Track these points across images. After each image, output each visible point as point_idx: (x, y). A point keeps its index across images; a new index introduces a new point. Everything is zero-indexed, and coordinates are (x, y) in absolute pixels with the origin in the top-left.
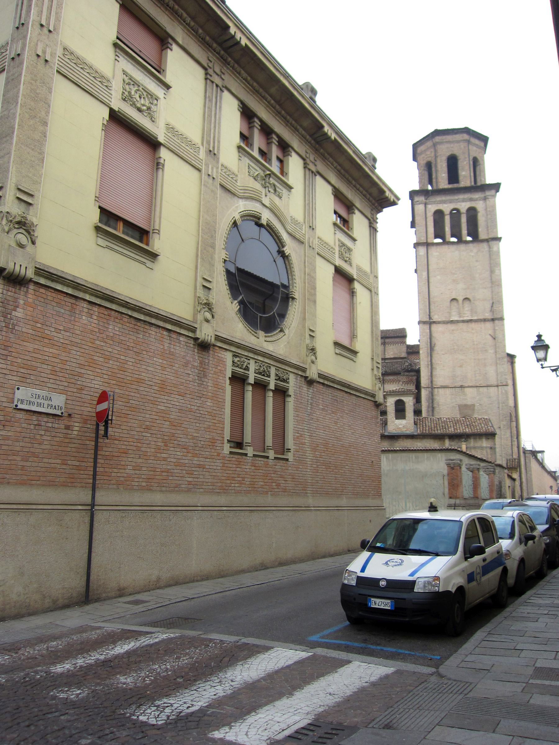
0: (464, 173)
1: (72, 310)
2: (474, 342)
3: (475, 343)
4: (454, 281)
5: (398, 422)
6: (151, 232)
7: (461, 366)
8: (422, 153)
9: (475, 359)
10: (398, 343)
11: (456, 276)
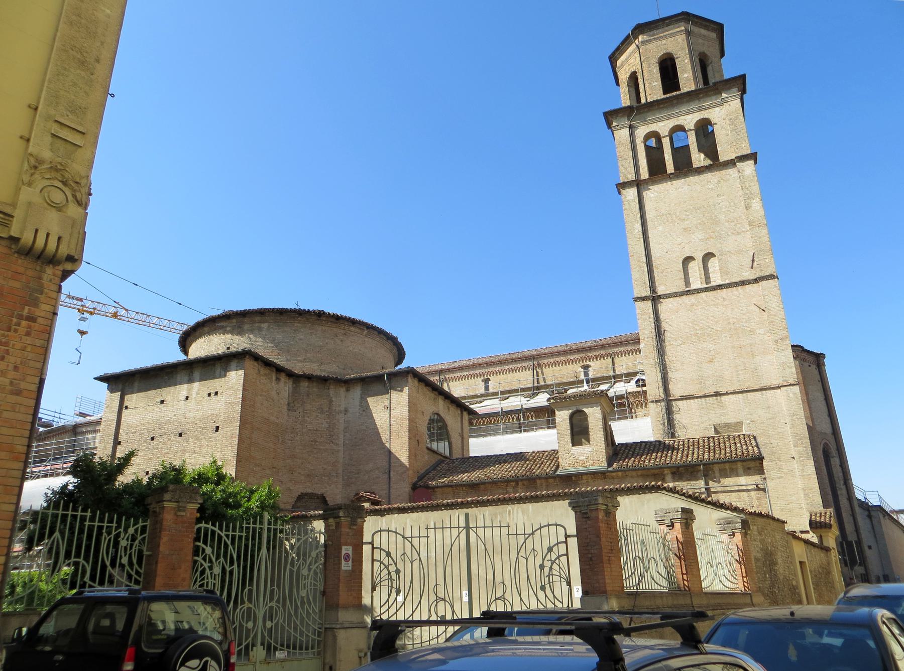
0: (685, 75)
1: (278, 379)
2: (729, 319)
3: (731, 320)
4: (685, 230)
5: (577, 450)
7: (711, 361)
8: (622, 65)
9: (733, 347)
11: (688, 222)
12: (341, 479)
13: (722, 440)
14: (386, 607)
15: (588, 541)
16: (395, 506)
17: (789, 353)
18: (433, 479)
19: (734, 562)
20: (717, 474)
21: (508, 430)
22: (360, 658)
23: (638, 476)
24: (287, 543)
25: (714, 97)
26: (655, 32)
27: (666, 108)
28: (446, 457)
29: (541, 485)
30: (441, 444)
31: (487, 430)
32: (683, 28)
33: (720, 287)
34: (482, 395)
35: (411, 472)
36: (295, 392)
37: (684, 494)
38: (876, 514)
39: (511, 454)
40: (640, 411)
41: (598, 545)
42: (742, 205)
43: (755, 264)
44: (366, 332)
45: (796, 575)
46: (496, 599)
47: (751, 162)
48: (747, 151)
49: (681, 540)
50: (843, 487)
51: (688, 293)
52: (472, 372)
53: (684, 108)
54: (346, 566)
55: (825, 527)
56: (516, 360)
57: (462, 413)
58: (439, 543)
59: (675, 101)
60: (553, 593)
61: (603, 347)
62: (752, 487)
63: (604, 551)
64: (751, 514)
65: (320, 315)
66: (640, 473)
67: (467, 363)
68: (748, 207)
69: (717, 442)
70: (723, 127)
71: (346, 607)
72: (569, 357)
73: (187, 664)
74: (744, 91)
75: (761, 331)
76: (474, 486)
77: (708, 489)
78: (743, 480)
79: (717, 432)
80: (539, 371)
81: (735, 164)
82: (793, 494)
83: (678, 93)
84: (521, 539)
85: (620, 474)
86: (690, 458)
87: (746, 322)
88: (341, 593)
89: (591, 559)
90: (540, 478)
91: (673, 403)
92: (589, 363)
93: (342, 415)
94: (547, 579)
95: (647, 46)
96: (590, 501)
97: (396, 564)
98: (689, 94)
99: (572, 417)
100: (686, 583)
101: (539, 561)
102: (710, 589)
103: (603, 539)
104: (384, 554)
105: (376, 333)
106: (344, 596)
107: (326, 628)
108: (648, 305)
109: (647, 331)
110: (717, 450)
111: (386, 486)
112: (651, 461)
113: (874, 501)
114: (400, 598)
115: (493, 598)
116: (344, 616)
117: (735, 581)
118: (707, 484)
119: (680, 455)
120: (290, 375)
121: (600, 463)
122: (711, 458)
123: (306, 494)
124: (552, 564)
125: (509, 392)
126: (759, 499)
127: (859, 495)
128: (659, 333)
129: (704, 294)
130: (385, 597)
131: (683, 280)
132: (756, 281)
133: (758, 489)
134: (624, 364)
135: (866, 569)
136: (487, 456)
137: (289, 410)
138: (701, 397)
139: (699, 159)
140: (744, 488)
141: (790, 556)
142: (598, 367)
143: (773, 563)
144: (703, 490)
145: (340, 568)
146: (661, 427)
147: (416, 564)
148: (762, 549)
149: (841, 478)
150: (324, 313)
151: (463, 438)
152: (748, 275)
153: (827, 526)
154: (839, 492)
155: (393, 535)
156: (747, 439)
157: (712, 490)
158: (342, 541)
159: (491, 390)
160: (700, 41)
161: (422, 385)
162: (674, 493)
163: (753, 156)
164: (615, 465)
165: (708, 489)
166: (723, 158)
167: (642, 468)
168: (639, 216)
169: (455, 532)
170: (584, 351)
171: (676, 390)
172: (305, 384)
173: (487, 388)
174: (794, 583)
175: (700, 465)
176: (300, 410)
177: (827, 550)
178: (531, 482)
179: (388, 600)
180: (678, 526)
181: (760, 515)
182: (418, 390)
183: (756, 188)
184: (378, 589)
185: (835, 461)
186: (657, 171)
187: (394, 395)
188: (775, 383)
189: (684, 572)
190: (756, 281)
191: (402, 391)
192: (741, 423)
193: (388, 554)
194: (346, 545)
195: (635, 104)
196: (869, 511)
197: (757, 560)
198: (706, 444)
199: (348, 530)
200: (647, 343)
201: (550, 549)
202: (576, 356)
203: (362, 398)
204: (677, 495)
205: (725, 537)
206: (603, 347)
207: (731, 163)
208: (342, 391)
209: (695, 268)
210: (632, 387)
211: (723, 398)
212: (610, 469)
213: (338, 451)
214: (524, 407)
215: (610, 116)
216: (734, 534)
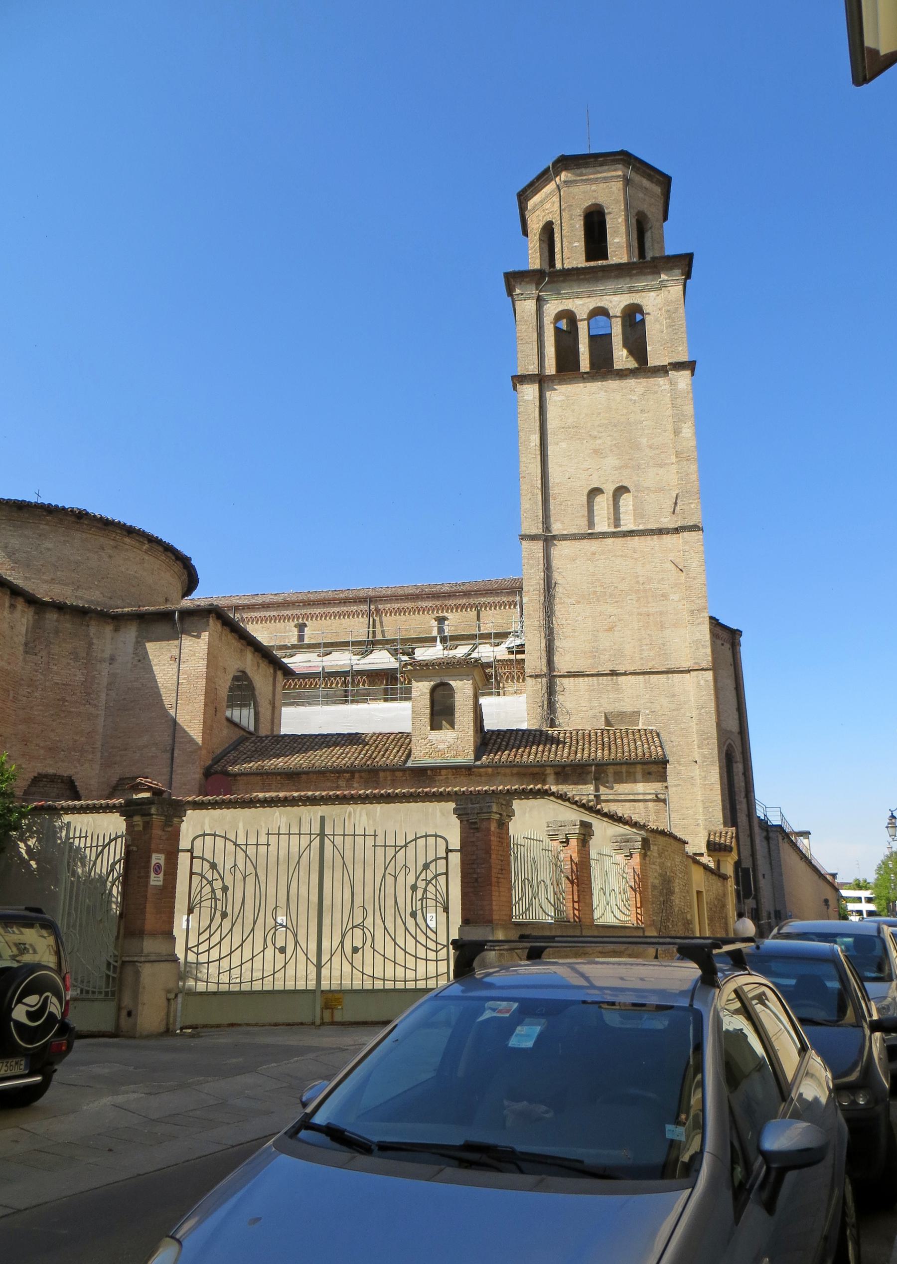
0: (617, 240)
1: (13, 607)
2: (637, 577)
3: (641, 580)
4: (596, 451)
5: (435, 735)
6: (665, 784)
8: (534, 209)
9: (639, 614)
10: (502, 605)
11: (599, 441)
12: (99, 755)
13: (618, 734)
14: (205, 936)
15: (474, 857)
16: (190, 799)
17: (706, 628)
18: (234, 763)
19: (628, 889)
20: (611, 779)
21: (330, 700)
22: (168, 1000)
23: (512, 775)
24: (22, 845)
25: (650, 277)
26: (584, 171)
27: (588, 280)
28: (250, 733)
29: (385, 779)
30: (245, 712)
31: (299, 696)
32: (620, 173)
33: (631, 533)
34: (294, 647)
35: (204, 752)
36: (36, 626)
37: (576, 803)
38: (777, 837)
39: (344, 735)
40: (510, 687)
41: (484, 862)
42: (670, 427)
43: (678, 508)
44: (146, 546)
45: (691, 907)
46: (353, 927)
47: (687, 373)
48: (684, 358)
49: (576, 860)
50: (744, 801)
51: (591, 536)
52: (282, 613)
53: (611, 285)
54: (156, 880)
55: (725, 850)
56: (345, 601)
57: (275, 672)
58: (283, 853)
59: (600, 274)
60: (425, 920)
61: (467, 594)
62: (650, 797)
63: (494, 871)
64: (653, 831)
65: (80, 517)
66: (515, 770)
67: (276, 599)
68: (677, 432)
69: (612, 737)
70: (657, 320)
71: (153, 934)
72: (420, 604)
73: (24, 1001)
74: (688, 275)
75: (676, 597)
76: (292, 777)
77: (597, 797)
78: (641, 788)
79: (608, 723)
80: (377, 619)
81: (667, 372)
82: (693, 809)
83: (604, 263)
84: (391, 852)
85: (490, 770)
86: (579, 755)
87: (659, 582)
88: (148, 916)
89: (476, 880)
90: (384, 770)
91: (557, 679)
92: (446, 614)
93: (105, 665)
94: (419, 903)
95: (571, 189)
96: (481, 808)
97: (223, 879)
98: (619, 267)
99: (433, 690)
100: (576, 912)
101: (411, 880)
102: (601, 922)
103: (493, 856)
104: (206, 866)
105: (161, 549)
106: (151, 921)
107: (124, 962)
108: (539, 546)
109: (534, 582)
110: (613, 747)
111: (166, 770)
112: (531, 755)
113: (775, 820)
114: (227, 924)
115: (350, 926)
116: (150, 946)
117: (627, 912)
118: (597, 790)
119: (566, 750)
120: (32, 601)
121: (466, 756)
122: (606, 758)
123: (46, 776)
124: (427, 885)
125: (332, 645)
126: (657, 812)
127: (760, 813)
128: (549, 586)
129: (610, 541)
130: (205, 923)
131: (586, 519)
132: (677, 530)
133: (658, 800)
134: (492, 620)
135: (758, 902)
136: (310, 736)
137: (26, 652)
138: (592, 675)
139: (621, 357)
140: (641, 797)
141: (688, 883)
142: (456, 621)
143: (671, 892)
144: (592, 797)
145: (147, 882)
146: (539, 710)
147: (250, 880)
148: (660, 875)
149: (743, 790)
150: (87, 514)
151: (274, 707)
152: (668, 522)
153: (727, 849)
154: (738, 807)
155: (220, 842)
156: (649, 736)
157: (602, 798)
158: (153, 846)
159: (306, 641)
160: (641, 195)
161: (227, 631)
162: (564, 800)
163: (690, 366)
164: (484, 758)
165: (597, 797)
166: (652, 361)
167: (516, 764)
168: (538, 424)
169: (305, 841)
170: (440, 598)
171: (563, 663)
172: (52, 617)
173: (301, 638)
174: (689, 917)
175: (591, 765)
176: (43, 653)
177: (724, 878)
178: (377, 775)
179: (209, 926)
180: (574, 843)
181: (663, 833)
182: (221, 636)
183: (689, 409)
184: (196, 911)
185: (738, 768)
186: (567, 365)
187: (187, 642)
188: (685, 665)
189: (639, 905)
190: (677, 530)
191: (198, 637)
192: (638, 713)
193: (213, 866)
194: (157, 852)
195: (547, 268)
196: (767, 831)
197: (654, 887)
198: (599, 739)
199: (160, 833)
200: (532, 597)
201: (426, 866)
202: (428, 604)
203: (137, 642)
204: (567, 803)
205: (620, 858)
206: (467, 594)
207: (662, 371)
208: (108, 630)
209: (603, 503)
210: (501, 652)
211: (621, 679)
212: (478, 763)
213: (97, 716)
214: (356, 668)
215: (514, 279)
216: (631, 855)
